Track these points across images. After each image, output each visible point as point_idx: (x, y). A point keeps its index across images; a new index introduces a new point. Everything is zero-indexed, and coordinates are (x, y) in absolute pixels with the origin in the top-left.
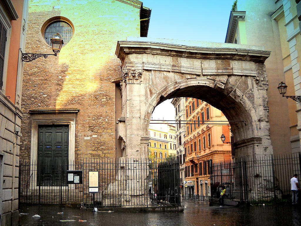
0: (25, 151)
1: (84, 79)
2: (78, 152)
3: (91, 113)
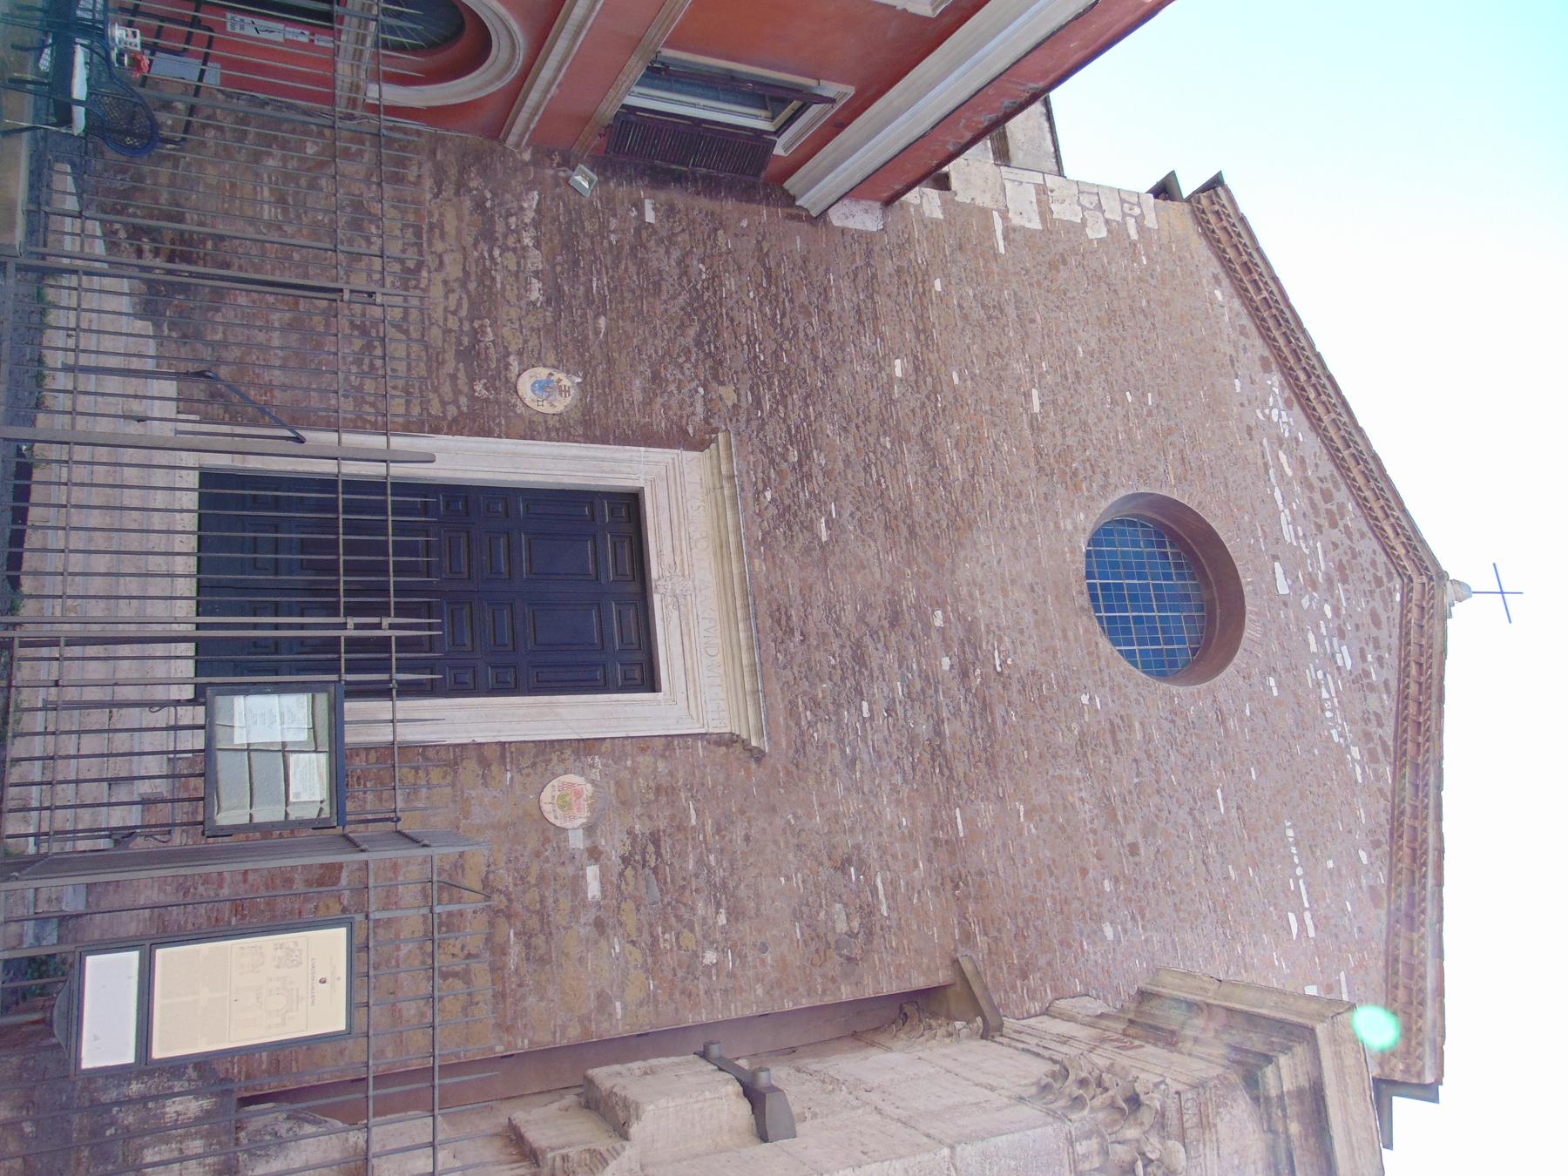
0: (463, 400)
1: (946, 772)
2: (471, 766)
3: (747, 839)
